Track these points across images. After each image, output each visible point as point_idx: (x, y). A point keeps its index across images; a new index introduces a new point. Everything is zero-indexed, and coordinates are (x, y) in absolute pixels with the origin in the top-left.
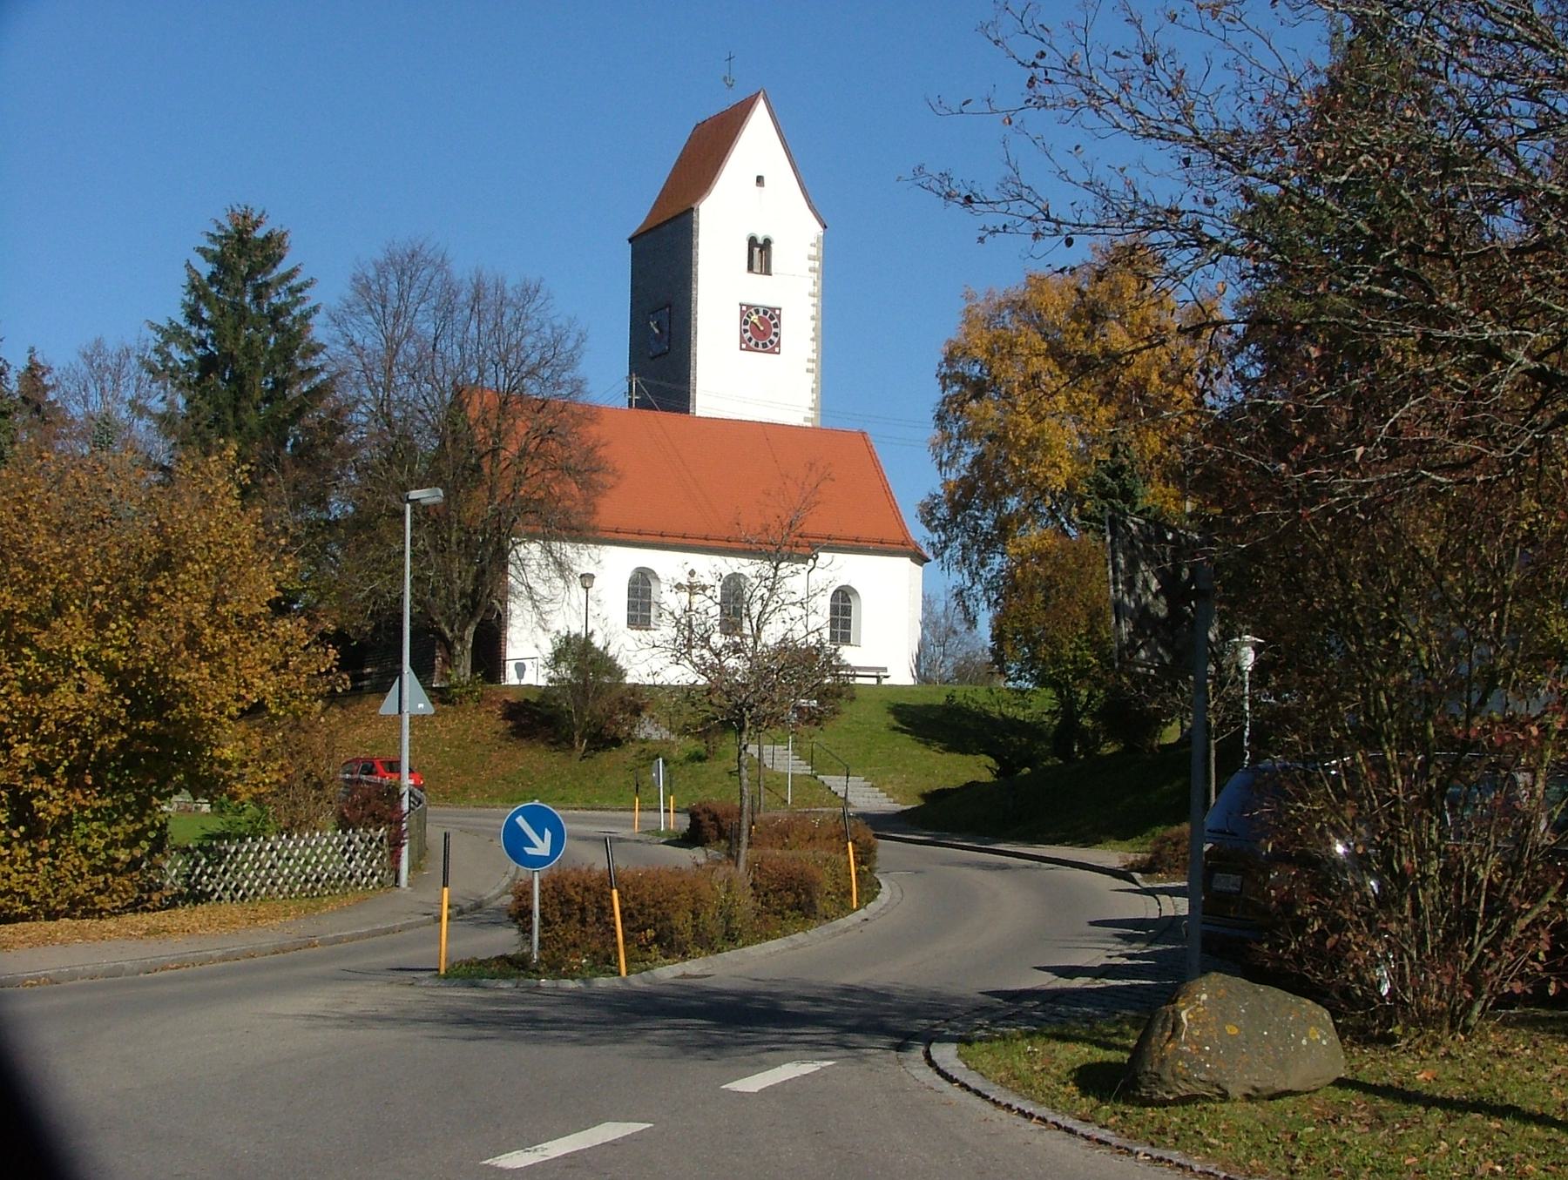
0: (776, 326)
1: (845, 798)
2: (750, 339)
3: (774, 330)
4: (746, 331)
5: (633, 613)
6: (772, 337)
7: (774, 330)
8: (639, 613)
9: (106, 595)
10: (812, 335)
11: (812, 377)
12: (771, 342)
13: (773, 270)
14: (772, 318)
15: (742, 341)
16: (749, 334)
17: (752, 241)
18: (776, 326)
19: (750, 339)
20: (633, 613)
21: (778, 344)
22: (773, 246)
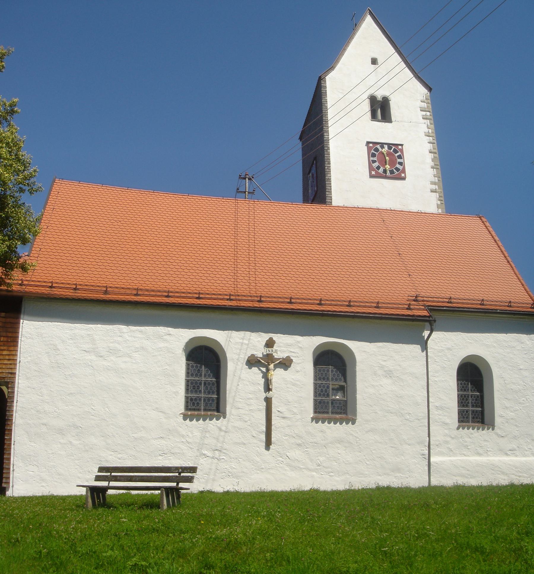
0: (400, 157)
1: (480, 218)
2: (378, 168)
3: (399, 160)
4: (374, 162)
5: (194, 395)
6: (398, 166)
7: (399, 160)
8: (202, 395)
9: (93, 526)
10: (432, 164)
11: (435, 196)
12: (397, 169)
13: (393, 119)
14: (396, 151)
15: (371, 168)
16: (376, 164)
17: (373, 99)
18: (400, 157)
19: (378, 168)
20: (194, 395)
21: (404, 171)
22: (391, 103)
